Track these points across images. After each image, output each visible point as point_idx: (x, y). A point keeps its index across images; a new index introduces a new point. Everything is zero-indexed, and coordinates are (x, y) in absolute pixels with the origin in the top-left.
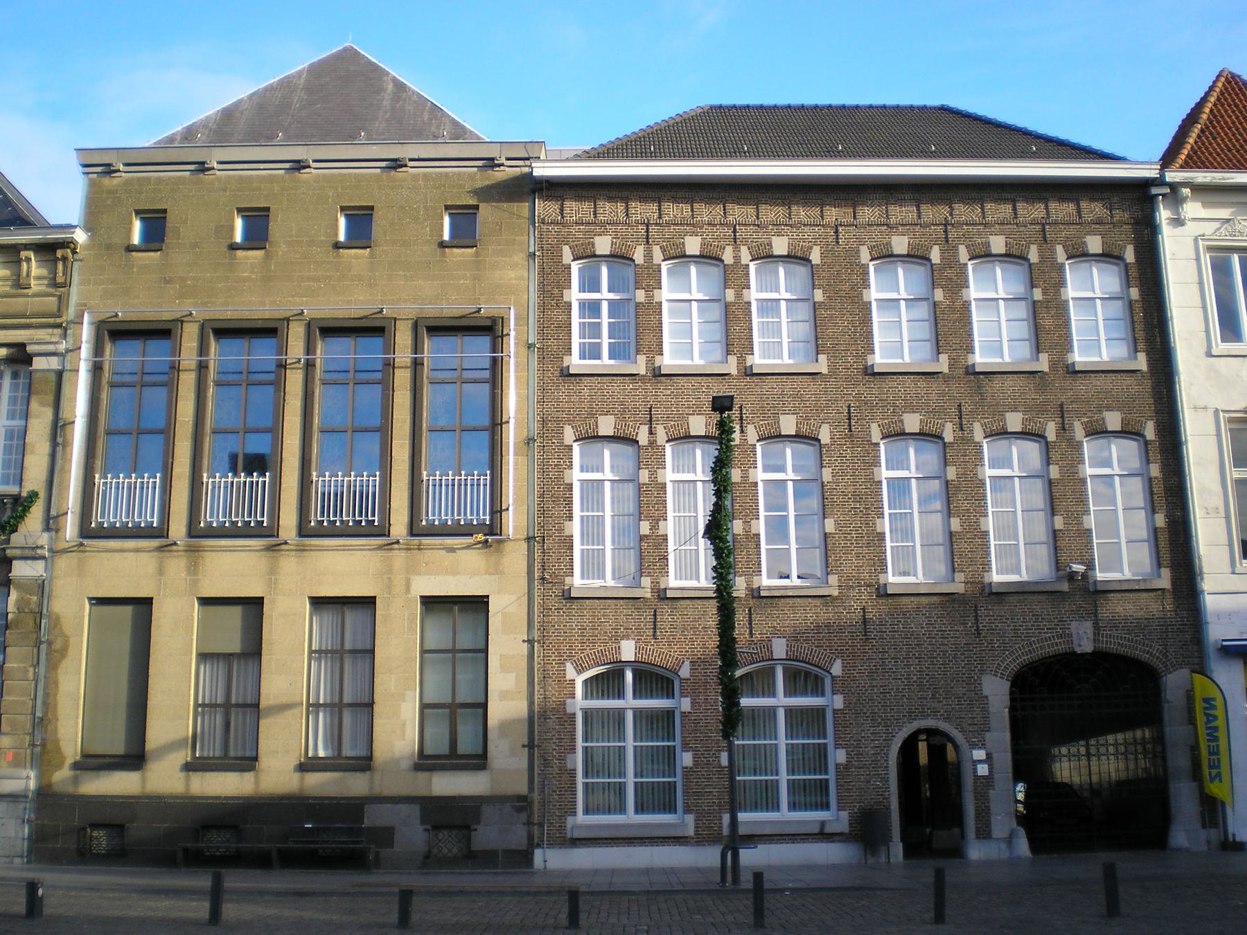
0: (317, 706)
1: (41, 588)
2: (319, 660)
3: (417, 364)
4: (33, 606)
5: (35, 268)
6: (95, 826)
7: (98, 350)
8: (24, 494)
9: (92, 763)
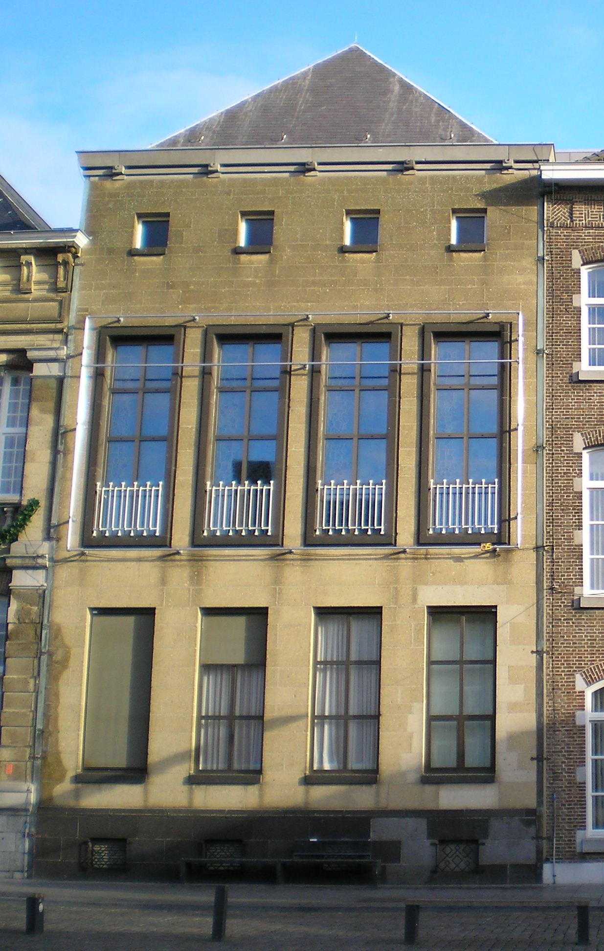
0: (322, 718)
1: (42, 597)
2: (324, 671)
3: (424, 370)
4: (33, 617)
5: (35, 273)
6: (96, 840)
7: (100, 356)
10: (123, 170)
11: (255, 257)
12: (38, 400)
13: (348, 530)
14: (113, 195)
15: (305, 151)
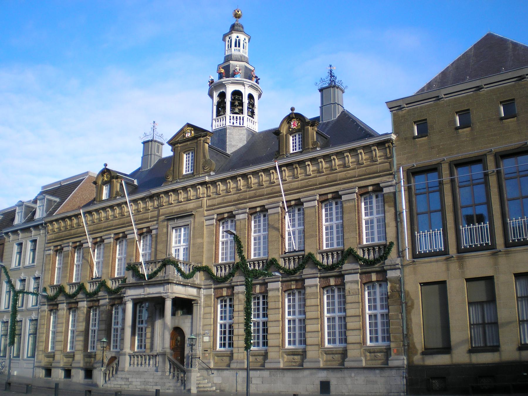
0: (523, 321)
1: (400, 281)
2: (522, 301)
3: (452, 181)
4: (398, 289)
5: (378, 153)
6: (433, 378)
7: (408, 181)
8: (388, 244)
9: (428, 352)
10: (405, 106)
11: (465, 130)
12: (387, 203)
13: (524, 239)
14: (403, 116)
15: (477, 81)
